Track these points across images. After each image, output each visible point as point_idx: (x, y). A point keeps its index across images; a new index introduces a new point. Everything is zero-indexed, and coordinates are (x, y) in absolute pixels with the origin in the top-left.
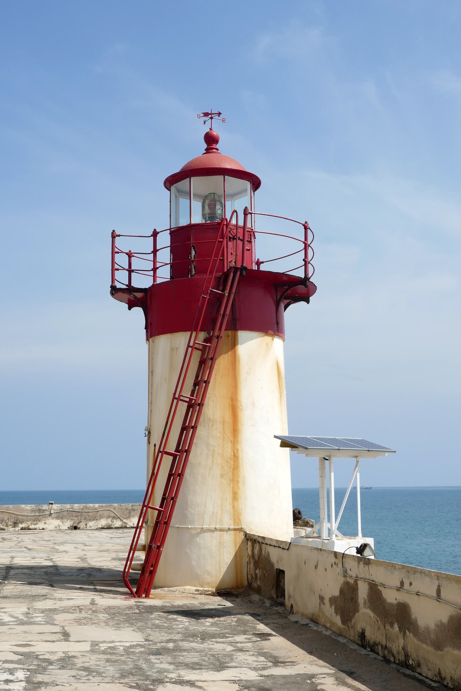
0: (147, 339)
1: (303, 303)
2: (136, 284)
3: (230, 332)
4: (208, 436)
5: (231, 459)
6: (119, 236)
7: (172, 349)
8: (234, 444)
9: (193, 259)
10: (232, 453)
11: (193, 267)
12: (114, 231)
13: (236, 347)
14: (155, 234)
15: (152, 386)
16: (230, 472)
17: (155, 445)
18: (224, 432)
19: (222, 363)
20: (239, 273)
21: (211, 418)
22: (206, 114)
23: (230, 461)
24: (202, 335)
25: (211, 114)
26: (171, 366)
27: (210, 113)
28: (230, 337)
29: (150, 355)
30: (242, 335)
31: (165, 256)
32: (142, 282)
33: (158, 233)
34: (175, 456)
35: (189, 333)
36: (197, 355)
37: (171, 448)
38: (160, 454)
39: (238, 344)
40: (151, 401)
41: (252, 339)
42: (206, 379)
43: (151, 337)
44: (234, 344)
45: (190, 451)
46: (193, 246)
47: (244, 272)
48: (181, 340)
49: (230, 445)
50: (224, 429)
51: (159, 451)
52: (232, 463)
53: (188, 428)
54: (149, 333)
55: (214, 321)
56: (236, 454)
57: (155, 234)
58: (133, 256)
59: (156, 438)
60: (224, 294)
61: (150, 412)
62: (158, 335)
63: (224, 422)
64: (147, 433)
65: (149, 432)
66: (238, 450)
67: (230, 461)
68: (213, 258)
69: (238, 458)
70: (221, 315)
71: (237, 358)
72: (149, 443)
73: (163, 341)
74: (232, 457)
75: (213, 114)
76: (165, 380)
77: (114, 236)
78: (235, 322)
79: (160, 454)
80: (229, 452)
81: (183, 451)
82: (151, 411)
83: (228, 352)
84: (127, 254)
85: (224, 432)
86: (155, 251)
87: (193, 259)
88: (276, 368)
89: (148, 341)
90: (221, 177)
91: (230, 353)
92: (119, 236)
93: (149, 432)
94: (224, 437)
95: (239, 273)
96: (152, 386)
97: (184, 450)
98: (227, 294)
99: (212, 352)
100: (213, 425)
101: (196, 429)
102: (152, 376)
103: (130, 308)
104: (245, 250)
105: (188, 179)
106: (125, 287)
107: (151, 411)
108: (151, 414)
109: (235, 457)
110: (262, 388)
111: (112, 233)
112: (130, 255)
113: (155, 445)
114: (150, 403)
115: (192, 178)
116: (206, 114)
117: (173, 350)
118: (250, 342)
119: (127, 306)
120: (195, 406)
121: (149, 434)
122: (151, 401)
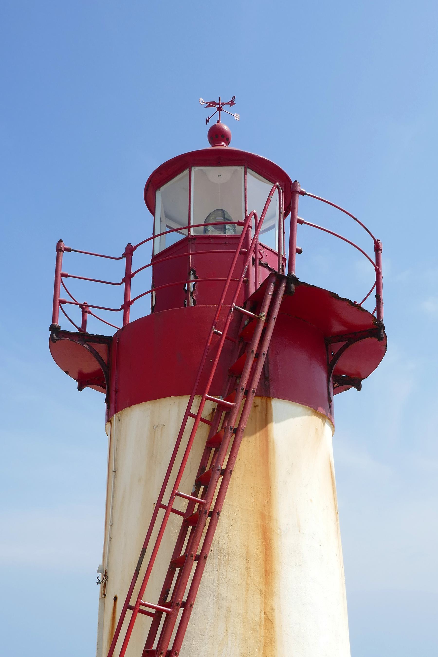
0: (109, 420)
1: (353, 389)
2: (93, 329)
3: (258, 400)
4: (218, 581)
5: (260, 626)
6: (69, 250)
7: (154, 428)
8: (265, 598)
9: (192, 289)
10: (263, 615)
11: (192, 301)
12: (61, 241)
13: (269, 426)
14: (129, 251)
15: (114, 496)
16: (259, 650)
17: (115, 599)
18: (248, 575)
19: (248, 446)
20: (284, 285)
21: (225, 547)
22: (211, 104)
23: (258, 629)
24: (209, 407)
25: (219, 104)
26: (152, 456)
27: (217, 102)
28: (259, 408)
29: (113, 439)
30: (278, 406)
31: (143, 281)
32: (104, 326)
33: (135, 248)
34: (157, 617)
35: (186, 400)
36: (203, 432)
37: (152, 597)
38: (129, 613)
39: (271, 421)
40: (112, 521)
41: (294, 416)
42: (224, 468)
43: (116, 412)
44: (265, 420)
45: (191, 606)
46: (193, 270)
47: (293, 286)
48: (171, 411)
49: (258, 598)
50: (247, 568)
51: (127, 606)
52: (263, 633)
53: (187, 561)
54: (113, 406)
55: (237, 372)
56: (270, 618)
57: (129, 251)
58: (90, 313)
59: (119, 587)
60: (259, 319)
61: (109, 539)
62: (130, 405)
63: (247, 557)
64: (101, 579)
65: (106, 576)
66: (272, 609)
67: (258, 629)
68: (230, 278)
69: (272, 623)
70: (253, 352)
71: (271, 446)
72: (105, 595)
73: (138, 416)
74: (263, 623)
75: (223, 104)
76: (139, 480)
77: (60, 249)
78: (266, 382)
79: (129, 613)
80: (256, 613)
81: (177, 605)
82: (111, 539)
83: (255, 433)
84: (81, 306)
85: (248, 575)
86: (128, 277)
87: (192, 289)
88: (330, 471)
89: (109, 424)
90: (240, 170)
91: (258, 435)
92: (69, 250)
93: (106, 576)
94: (247, 584)
95: (284, 285)
96: (114, 496)
97: (180, 603)
98: (263, 319)
99: (236, 416)
100: (228, 561)
101: (205, 561)
102: (115, 478)
103: (80, 388)
104: (295, 250)
105: (187, 171)
106: (76, 331)
107: (111, 539)
108: (110, 543)
109: (268, 621)
110: (311, 501)
111: (58, 244)
112: (84, 308)
113: (115, 599)
114: (109, 524)
115: (193, 169)
116: (211, 104)
117: (156, 428)
118: (291, 420)
119: (76, 384)
120: (198, 520)
121: (105, 579)
122: (112, 521)
